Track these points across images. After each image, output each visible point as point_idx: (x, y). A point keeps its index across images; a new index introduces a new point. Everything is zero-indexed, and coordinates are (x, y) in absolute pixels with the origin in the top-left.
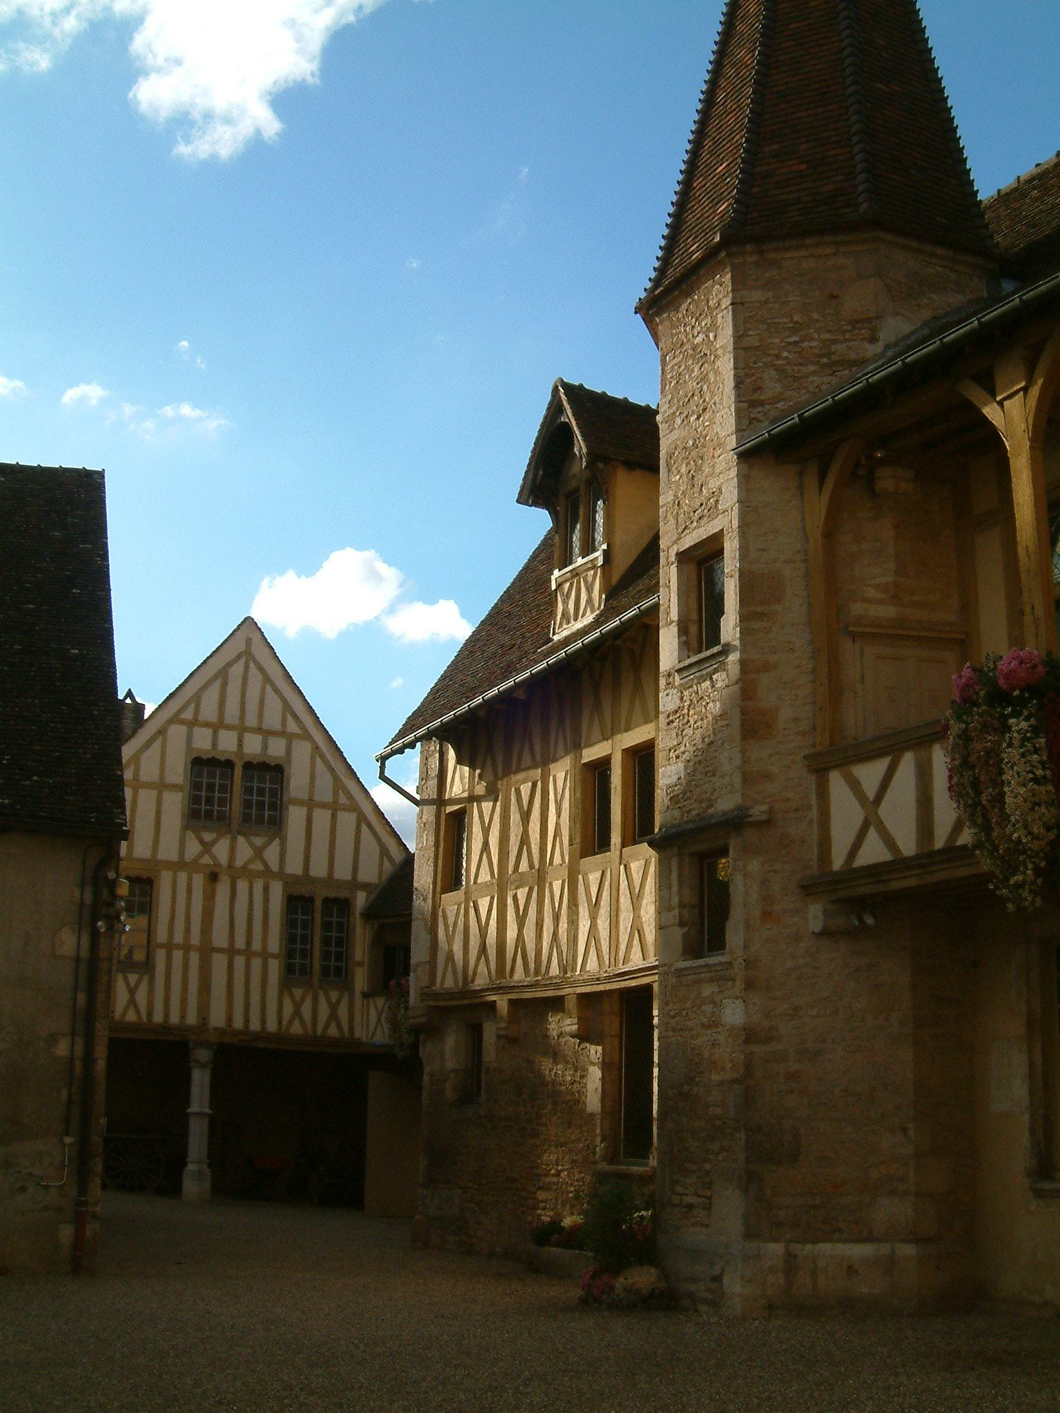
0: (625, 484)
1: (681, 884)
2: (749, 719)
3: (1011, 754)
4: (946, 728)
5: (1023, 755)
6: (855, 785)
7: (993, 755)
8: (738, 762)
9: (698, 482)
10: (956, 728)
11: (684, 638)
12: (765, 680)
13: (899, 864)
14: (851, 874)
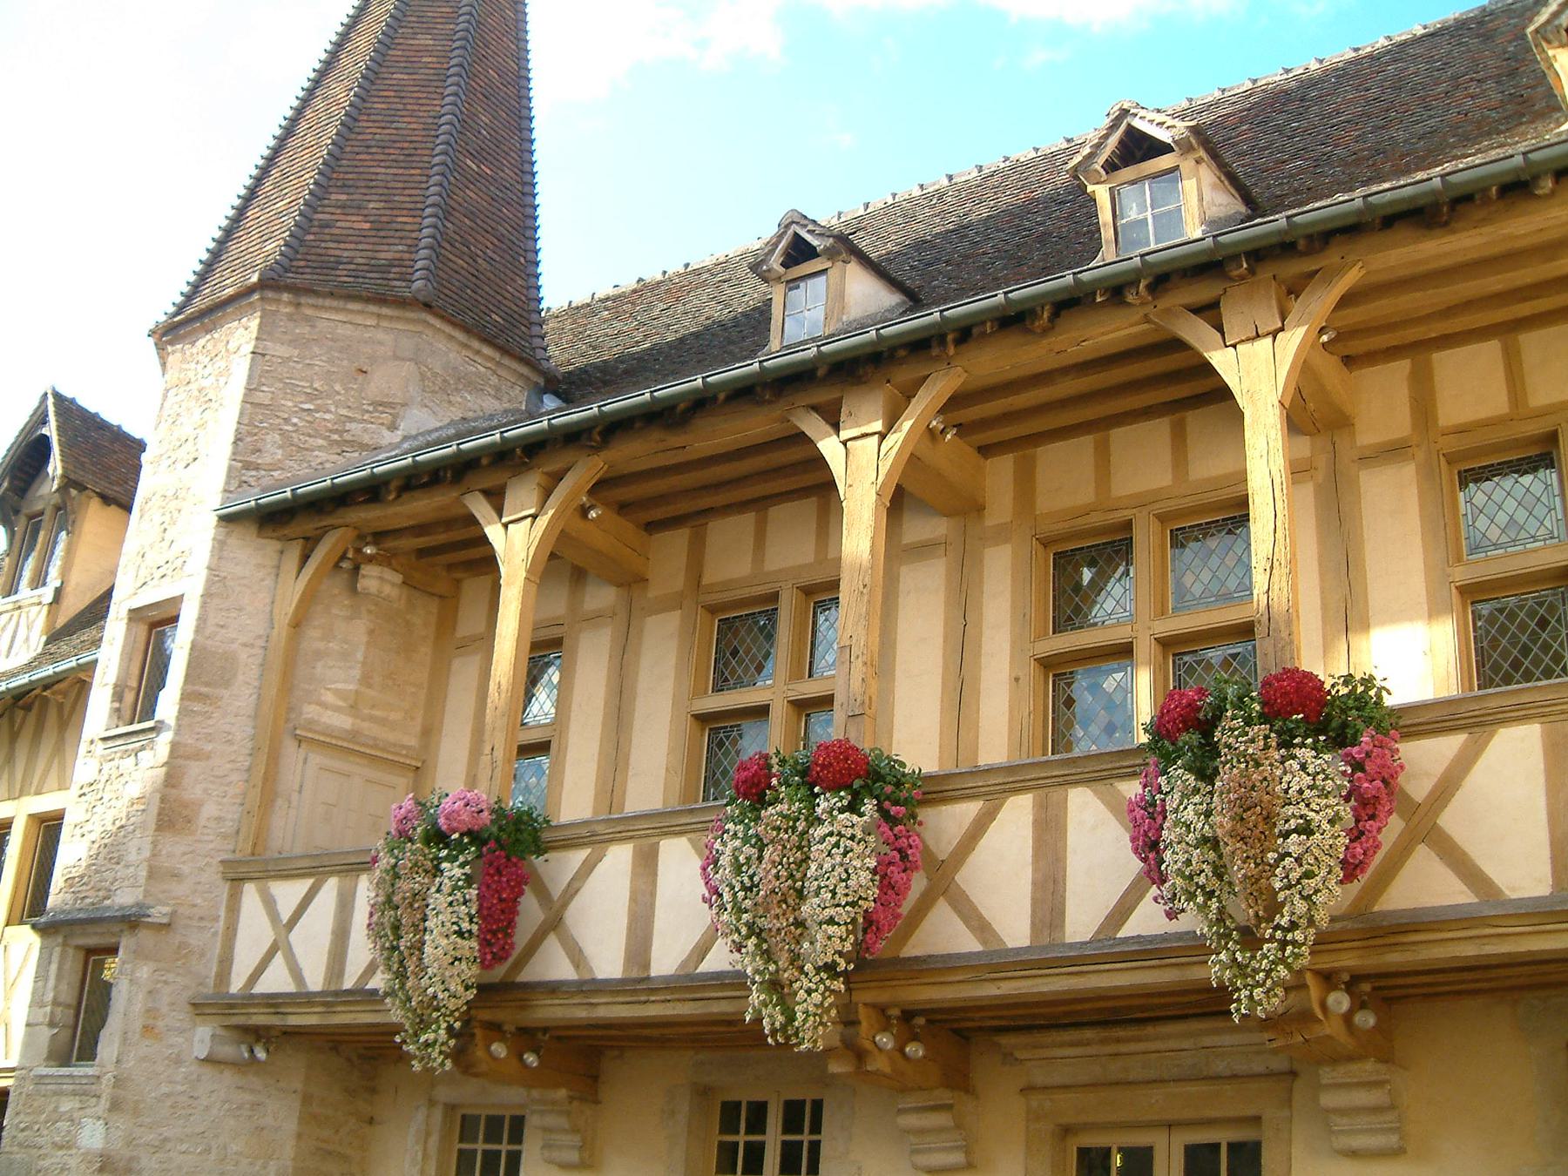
0: (94, 518)
1: (59, 977)
2: (170, 811)
3: (438, 900)
4: (375, 860)
5: (451, 904)
6: (270, 903)
7: (419, 896)
8: (147, 854)
9: (169, 537)
10: (385, 861)
11: (117, 705)
12: (194, 769)
13: (304, 999)
14: (249, 1000)
